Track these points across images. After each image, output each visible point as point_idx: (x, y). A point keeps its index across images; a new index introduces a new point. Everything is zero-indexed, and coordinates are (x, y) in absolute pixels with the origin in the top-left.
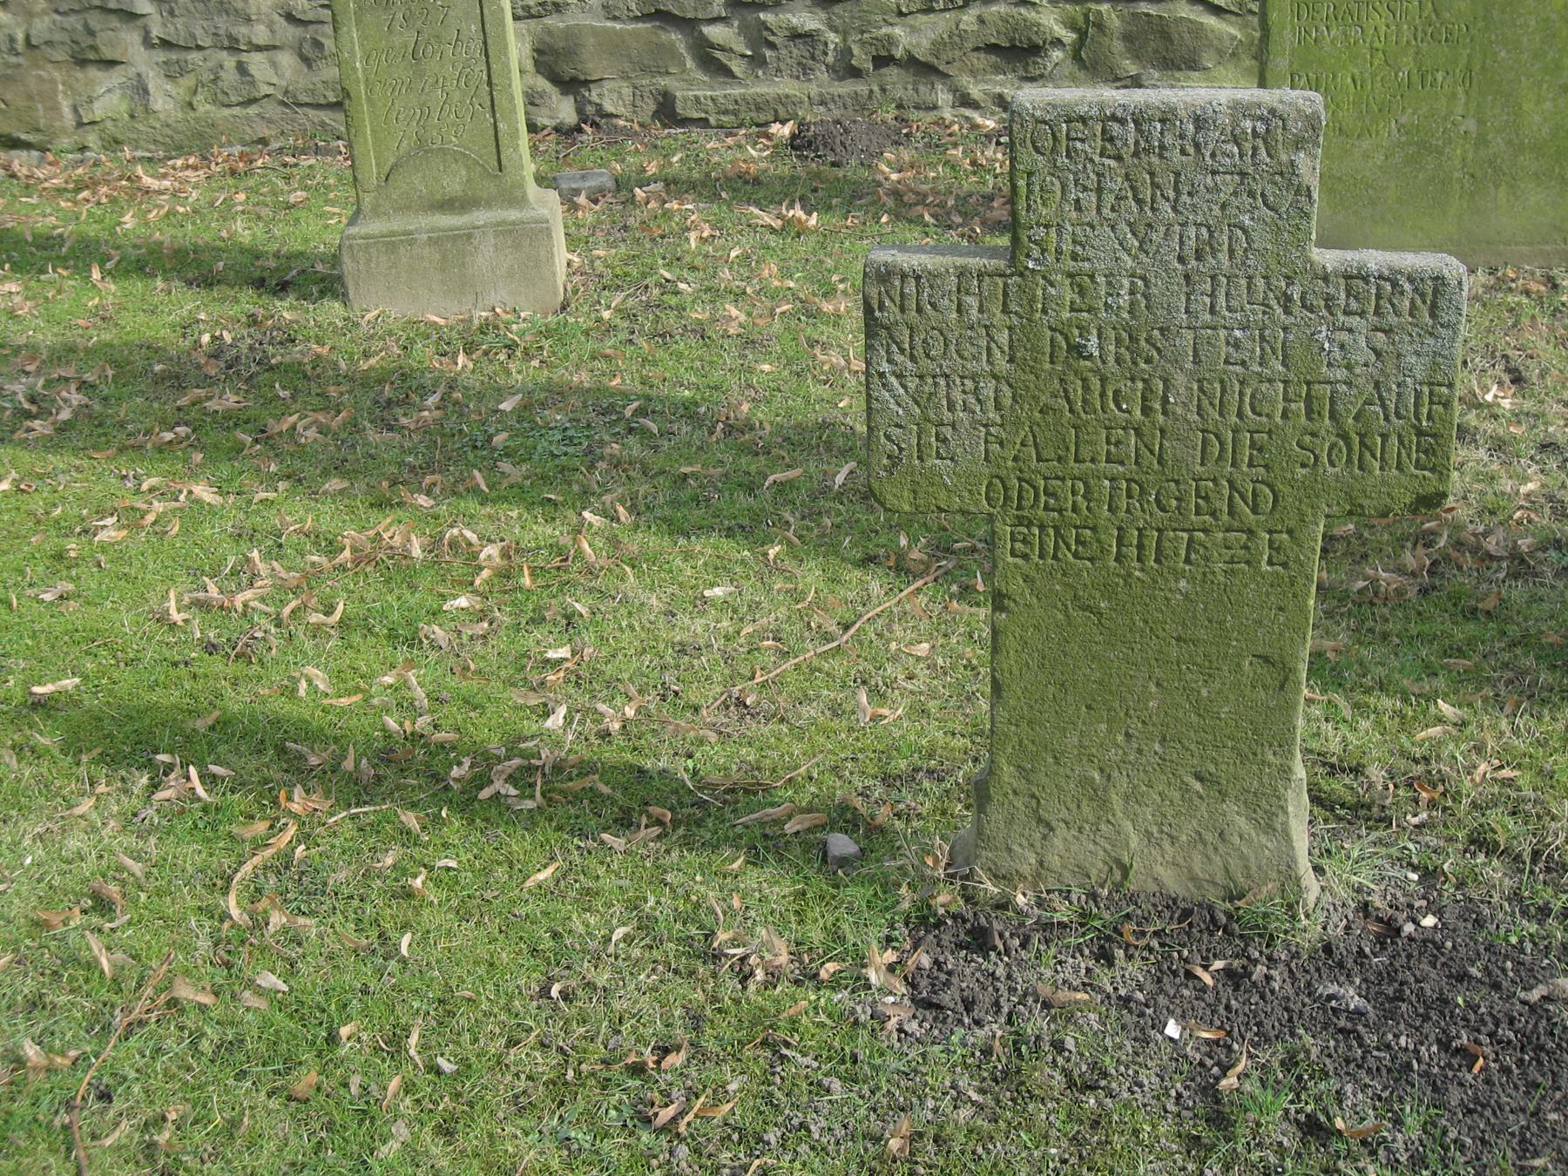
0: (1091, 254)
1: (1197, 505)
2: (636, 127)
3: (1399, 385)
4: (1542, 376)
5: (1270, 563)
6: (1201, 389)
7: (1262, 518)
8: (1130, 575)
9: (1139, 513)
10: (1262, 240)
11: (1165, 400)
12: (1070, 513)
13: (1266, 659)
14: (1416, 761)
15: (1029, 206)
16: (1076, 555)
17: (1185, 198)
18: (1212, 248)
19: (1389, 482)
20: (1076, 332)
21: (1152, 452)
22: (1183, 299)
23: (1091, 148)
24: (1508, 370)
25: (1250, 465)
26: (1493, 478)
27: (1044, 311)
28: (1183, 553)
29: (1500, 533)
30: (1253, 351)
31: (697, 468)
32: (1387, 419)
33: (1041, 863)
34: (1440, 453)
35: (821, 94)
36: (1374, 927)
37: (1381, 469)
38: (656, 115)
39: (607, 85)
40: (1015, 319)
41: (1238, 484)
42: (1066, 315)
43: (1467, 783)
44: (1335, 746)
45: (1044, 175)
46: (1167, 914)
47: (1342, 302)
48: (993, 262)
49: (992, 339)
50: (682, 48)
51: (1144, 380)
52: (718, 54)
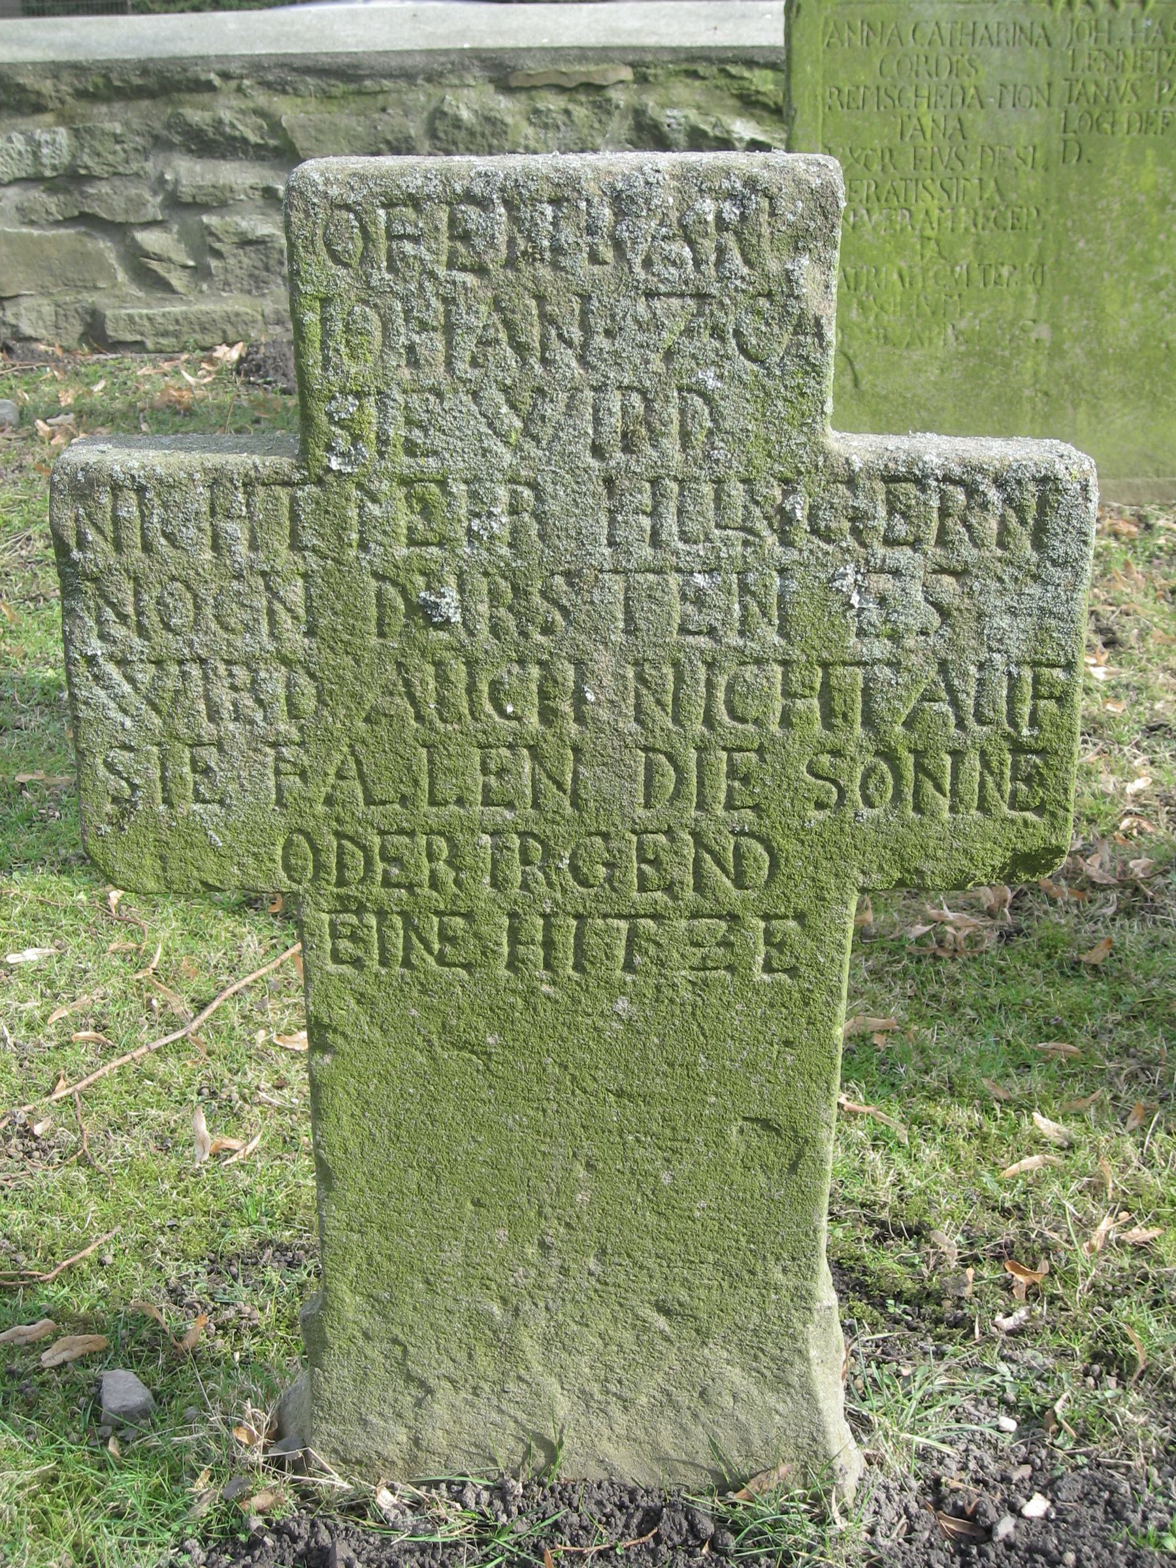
0: (439, 441)
1: (641, 875)
2: (59, 352)
3: (981, 667)
4: (1142, 636)
5: (768, 968)
6: (641, 678)
7: (752, 894)
8: (533, 991)
9: (544, 889)
10: (739, 414)
11: (579, 699)
12: (426, 891)
13: (766, 1124)
14: (1006, 1213)
15: (326, 360)
16: (441, 960)
17: (600, 341)
18: (651, 430)
19: (972, 834)
20: (420, 581)
21: (560, 786)
22: (604, 521)
23: (432, 254)
24: (1099, 631)
25: (730, 806)
26: (1089, 773)
27: (363, 546)
28: (621, 953)
29: (1105, 851)
30: (728, 611)
31: (41, 775)
32: (961, 724)
33: (416, 1442)
34: (1051, 781)
35: (277, 312)
36: (951, 1525)
37: (953, 809)
38: (84, 338)
39: (25, 303)
40: (313, 560)
41: (710, 839)
42: (401, 551)
43: (1083, 1251)
44: (886, 1194)
45: (350, 302)
46: (620, 1519)
47: (881, 524)
48: (270, 460)
49: (276, 595)
50: (112, 258)
51: (540, 663)
52: (154, 265)
